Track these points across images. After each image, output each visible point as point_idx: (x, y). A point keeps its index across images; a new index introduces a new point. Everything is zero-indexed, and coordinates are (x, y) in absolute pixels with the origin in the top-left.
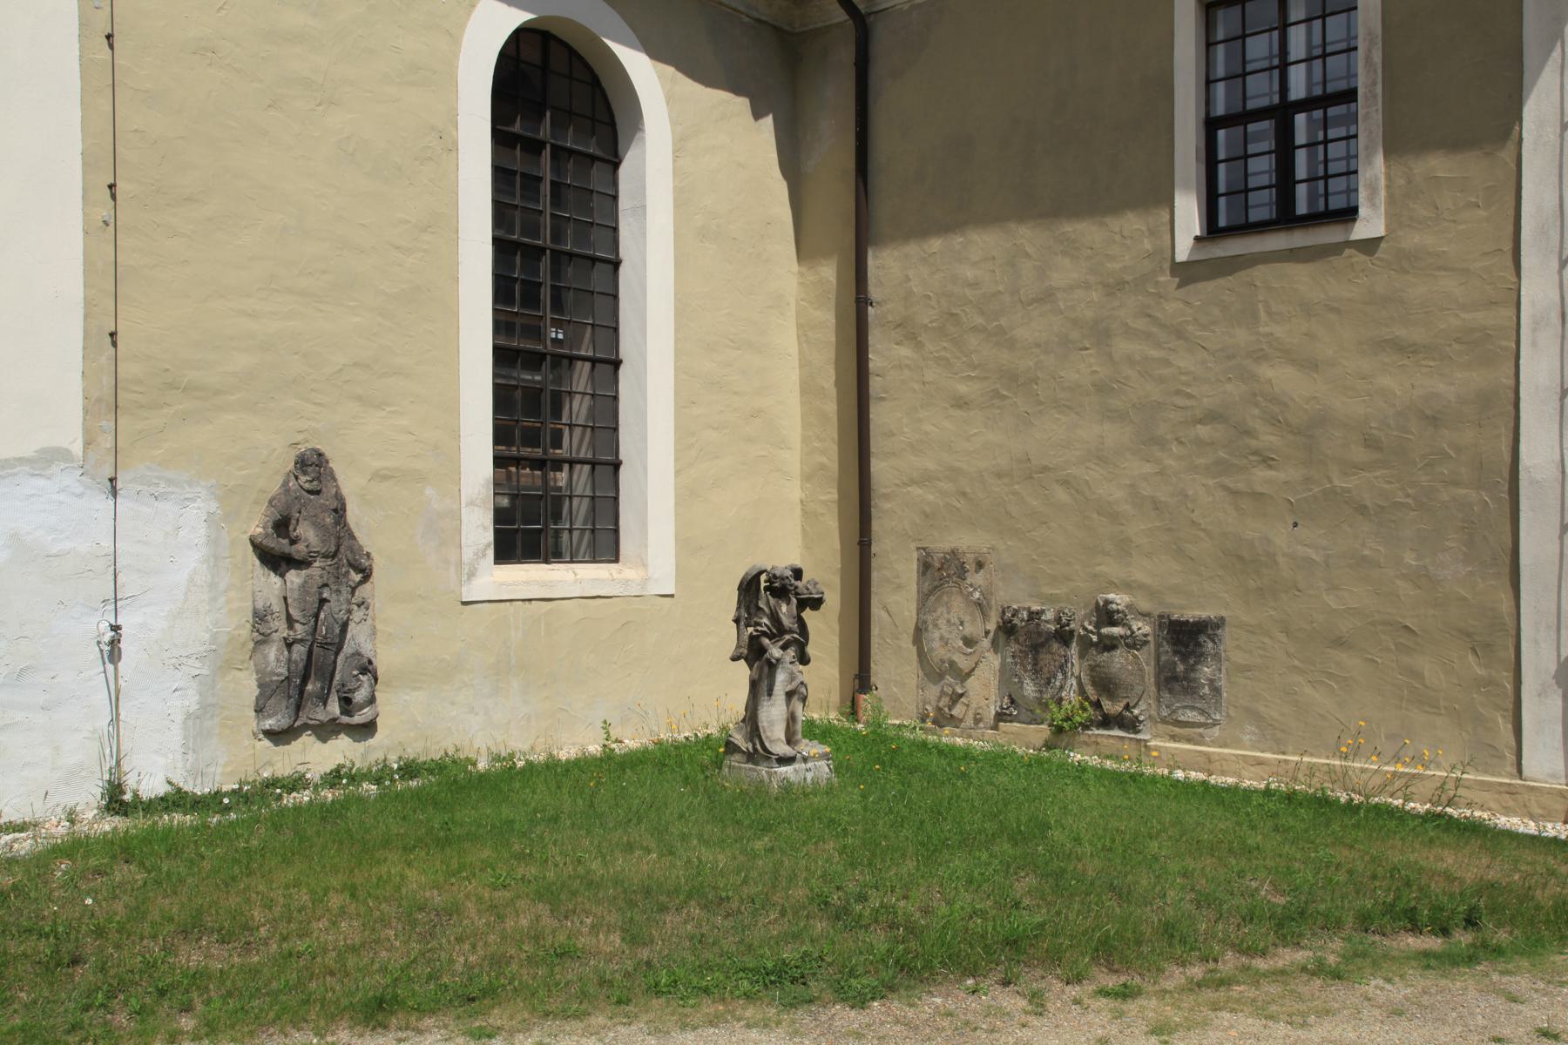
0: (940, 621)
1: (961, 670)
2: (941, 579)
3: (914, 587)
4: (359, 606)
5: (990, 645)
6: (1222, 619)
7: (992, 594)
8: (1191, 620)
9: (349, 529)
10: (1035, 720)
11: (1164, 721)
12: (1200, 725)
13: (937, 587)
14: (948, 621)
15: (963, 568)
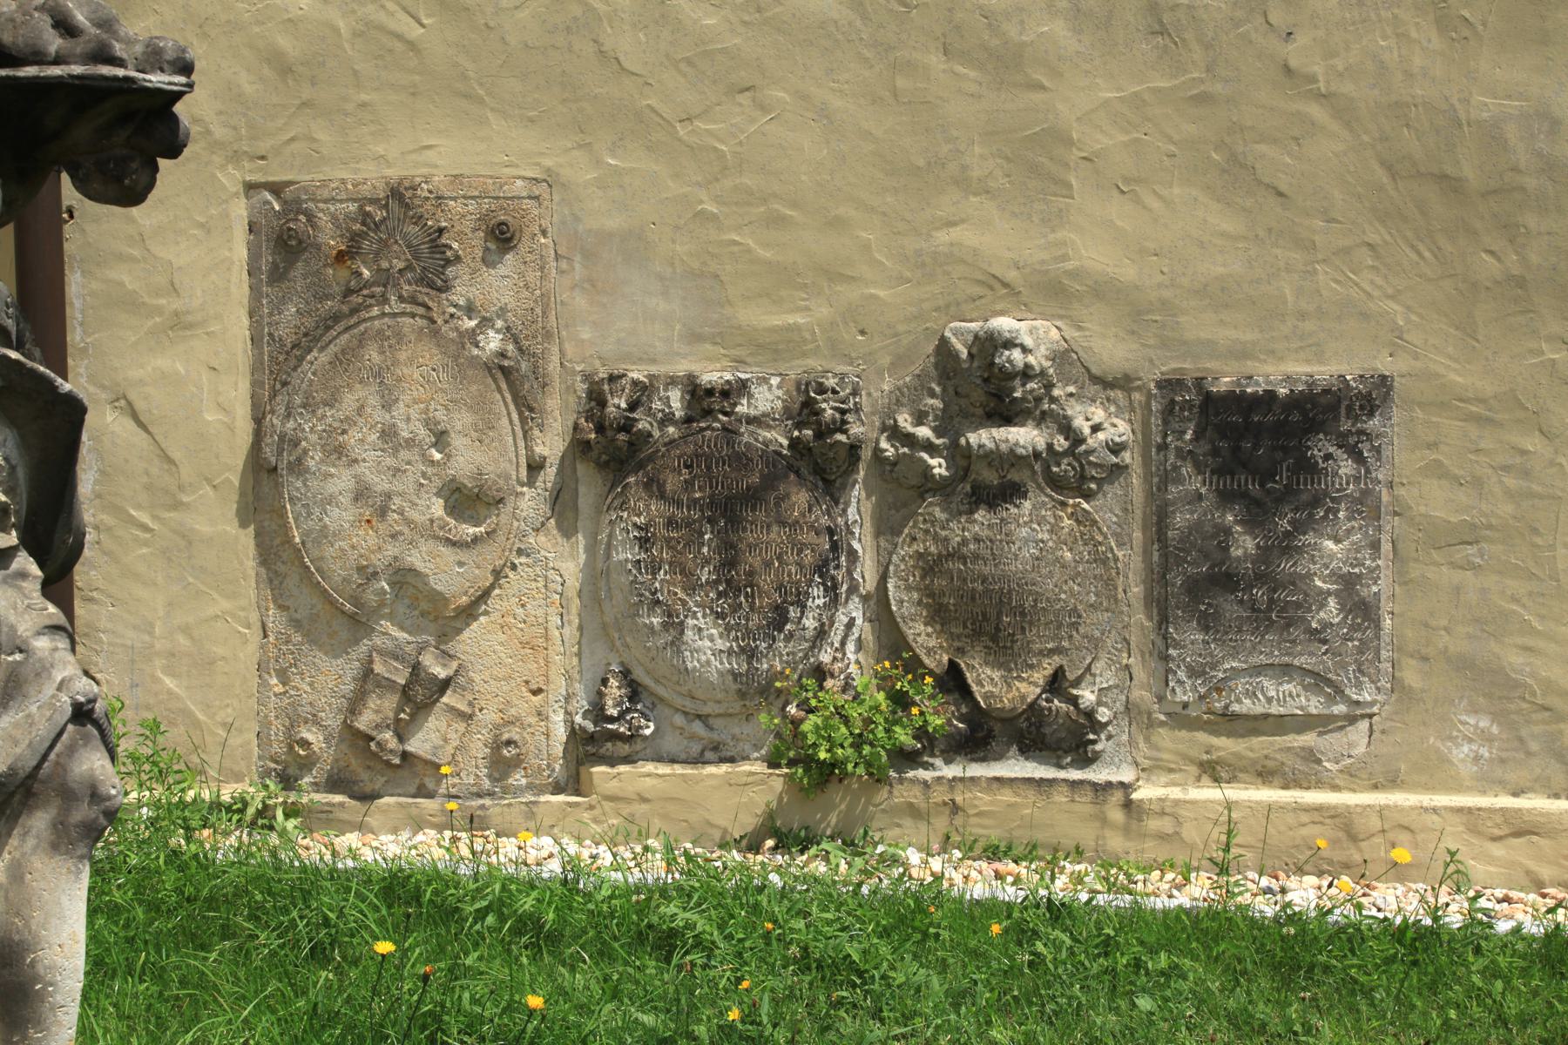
0: (352, 438)
1: (438, 599)
2: (349, 292)
3: (239, 325)
5: (545, 509)
6: (1384, 381)
7: (548, 335)
8: (1283, 391)
10: (715, 748)
11: (1180, 719)
12: (1306, 723)
13: (336, 318)
14: (388, 434)
15: (437, 247)
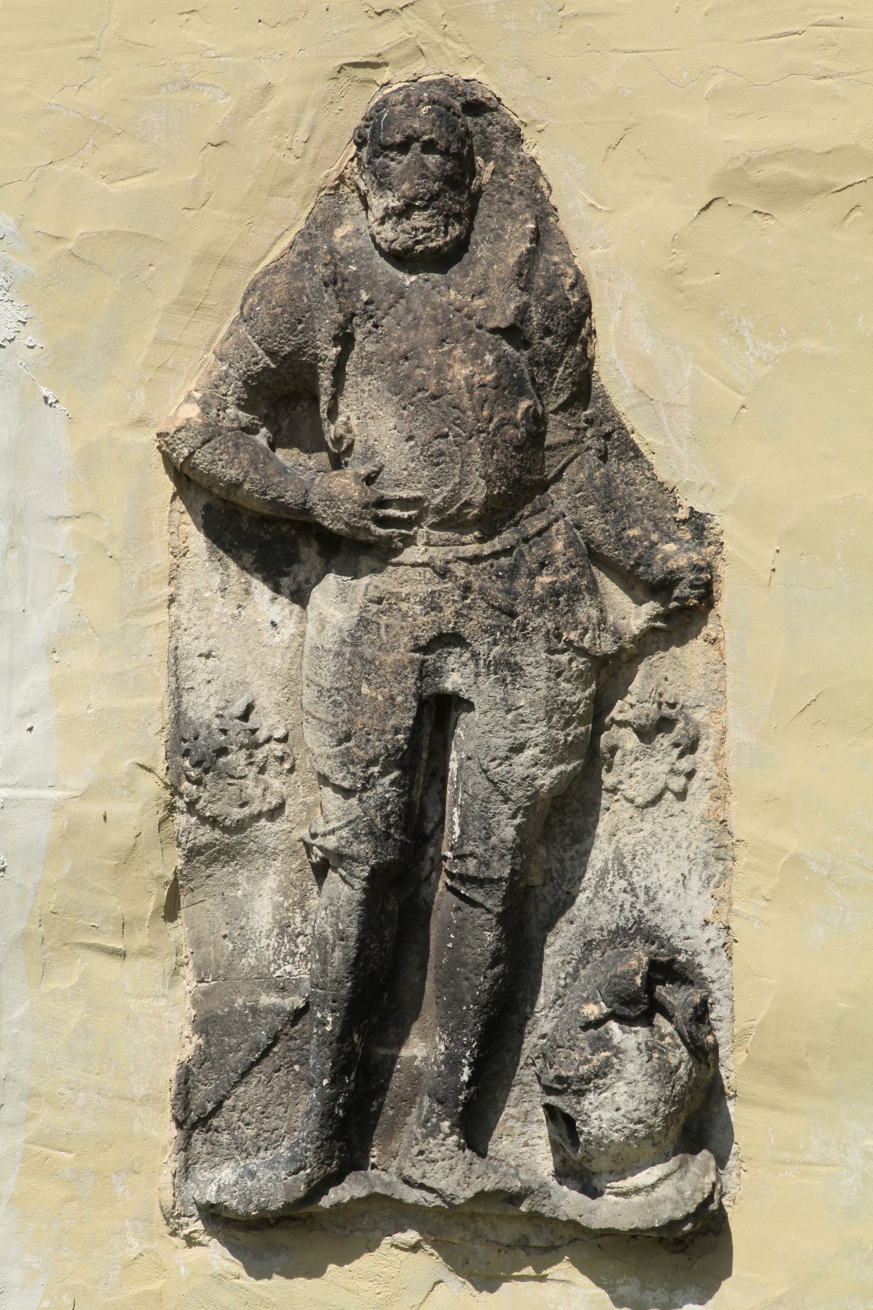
4: (646, 734)
9: (608, 415)
